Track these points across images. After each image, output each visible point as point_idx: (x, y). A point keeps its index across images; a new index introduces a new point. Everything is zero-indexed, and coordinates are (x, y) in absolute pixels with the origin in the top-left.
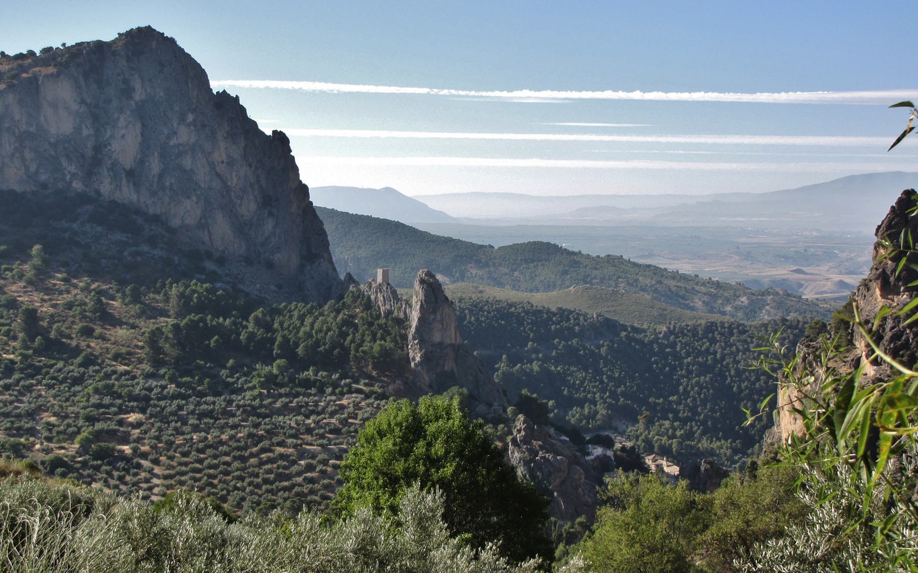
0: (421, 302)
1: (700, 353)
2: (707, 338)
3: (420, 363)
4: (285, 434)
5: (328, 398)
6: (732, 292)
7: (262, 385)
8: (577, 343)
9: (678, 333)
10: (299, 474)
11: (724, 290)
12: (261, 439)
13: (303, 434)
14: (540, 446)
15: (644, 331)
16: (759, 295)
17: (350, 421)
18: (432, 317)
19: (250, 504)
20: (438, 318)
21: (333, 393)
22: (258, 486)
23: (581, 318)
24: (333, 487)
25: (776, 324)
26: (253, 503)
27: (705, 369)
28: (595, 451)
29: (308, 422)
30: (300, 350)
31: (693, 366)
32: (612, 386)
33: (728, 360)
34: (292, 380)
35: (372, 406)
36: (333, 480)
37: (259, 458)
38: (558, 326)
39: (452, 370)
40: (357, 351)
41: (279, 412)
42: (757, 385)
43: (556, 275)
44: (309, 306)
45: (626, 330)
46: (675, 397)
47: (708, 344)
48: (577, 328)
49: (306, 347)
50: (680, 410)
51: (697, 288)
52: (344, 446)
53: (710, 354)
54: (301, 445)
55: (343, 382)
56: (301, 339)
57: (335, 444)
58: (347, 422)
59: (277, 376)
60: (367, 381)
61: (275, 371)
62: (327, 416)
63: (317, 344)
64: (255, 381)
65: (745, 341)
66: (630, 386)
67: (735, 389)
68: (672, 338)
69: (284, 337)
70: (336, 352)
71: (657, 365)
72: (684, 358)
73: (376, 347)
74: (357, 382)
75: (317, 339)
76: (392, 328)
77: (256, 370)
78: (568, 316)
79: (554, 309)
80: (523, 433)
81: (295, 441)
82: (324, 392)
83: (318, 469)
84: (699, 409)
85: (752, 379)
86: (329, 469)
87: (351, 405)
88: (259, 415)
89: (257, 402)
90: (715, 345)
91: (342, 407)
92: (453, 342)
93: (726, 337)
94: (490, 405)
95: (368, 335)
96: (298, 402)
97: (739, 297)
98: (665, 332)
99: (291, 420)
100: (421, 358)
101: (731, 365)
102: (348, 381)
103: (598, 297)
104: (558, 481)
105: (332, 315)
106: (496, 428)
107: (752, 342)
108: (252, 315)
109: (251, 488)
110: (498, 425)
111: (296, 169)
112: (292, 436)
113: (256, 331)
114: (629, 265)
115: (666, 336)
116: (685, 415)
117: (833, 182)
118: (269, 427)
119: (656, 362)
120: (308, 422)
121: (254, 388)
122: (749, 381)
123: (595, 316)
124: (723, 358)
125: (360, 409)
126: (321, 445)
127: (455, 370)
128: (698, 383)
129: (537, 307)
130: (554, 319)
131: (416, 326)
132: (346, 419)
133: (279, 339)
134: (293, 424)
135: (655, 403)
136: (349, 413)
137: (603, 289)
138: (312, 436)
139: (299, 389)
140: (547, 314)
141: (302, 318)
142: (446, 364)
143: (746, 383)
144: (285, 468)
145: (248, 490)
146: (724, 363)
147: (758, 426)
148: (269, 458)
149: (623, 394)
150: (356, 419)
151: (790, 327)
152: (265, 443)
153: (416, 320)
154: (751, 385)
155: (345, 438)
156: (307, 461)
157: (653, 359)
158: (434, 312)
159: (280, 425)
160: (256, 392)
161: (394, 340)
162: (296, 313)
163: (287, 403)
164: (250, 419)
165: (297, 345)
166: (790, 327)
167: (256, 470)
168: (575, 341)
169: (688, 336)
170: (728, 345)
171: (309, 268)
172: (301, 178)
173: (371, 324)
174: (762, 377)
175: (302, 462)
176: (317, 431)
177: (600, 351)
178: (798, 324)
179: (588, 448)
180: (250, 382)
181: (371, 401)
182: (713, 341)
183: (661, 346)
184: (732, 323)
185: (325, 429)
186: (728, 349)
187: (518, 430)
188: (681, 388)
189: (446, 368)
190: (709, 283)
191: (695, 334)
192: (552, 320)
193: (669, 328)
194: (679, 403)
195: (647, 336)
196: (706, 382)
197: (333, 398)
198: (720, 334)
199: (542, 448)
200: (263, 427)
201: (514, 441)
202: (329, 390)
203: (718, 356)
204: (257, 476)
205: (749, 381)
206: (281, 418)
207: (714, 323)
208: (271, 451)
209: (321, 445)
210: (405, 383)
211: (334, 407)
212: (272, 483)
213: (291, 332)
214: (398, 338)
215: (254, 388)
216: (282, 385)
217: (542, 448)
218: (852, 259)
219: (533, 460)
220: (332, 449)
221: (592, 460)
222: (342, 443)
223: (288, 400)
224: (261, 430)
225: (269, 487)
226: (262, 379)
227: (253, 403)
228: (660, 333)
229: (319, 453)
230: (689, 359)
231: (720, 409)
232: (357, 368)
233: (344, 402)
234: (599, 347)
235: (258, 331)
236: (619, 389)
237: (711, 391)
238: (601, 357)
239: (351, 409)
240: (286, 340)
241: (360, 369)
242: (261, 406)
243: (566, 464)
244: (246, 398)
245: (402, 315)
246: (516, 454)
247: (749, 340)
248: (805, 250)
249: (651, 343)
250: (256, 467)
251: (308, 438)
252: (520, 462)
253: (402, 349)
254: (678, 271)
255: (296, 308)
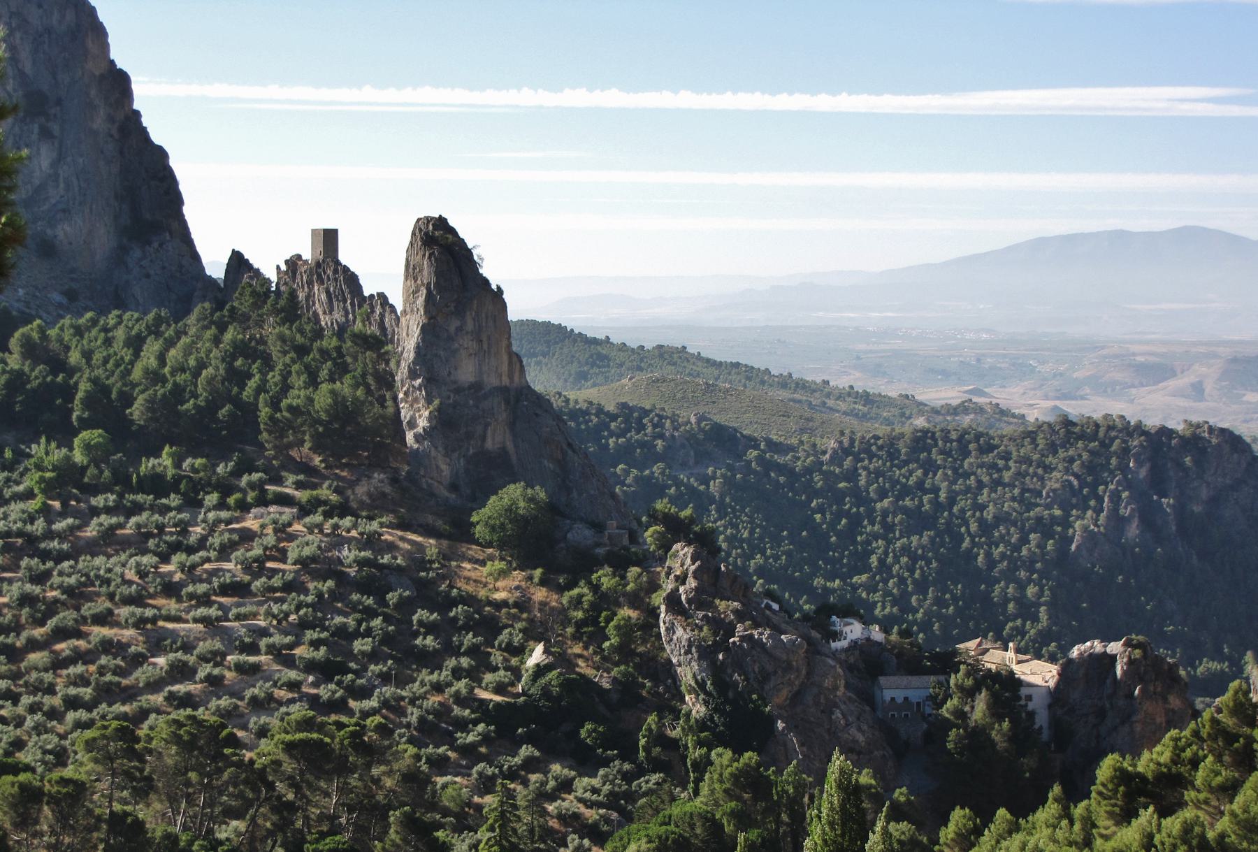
0: (428, 289)
1: (905, 491)
2: (917, 461)
3: (428, 434)
4: (111, 596)
5: (211, 515)
6: (896, 411)
7: (50, 488)
8: (663, 473)
9: (859, 453)
10: (154, 686)
11: (878, 407)
12: (52, 608)
13: (152, 596)
14: (735, 612)
15: (791, 449)
16: (948, 413)
17: (269, 565)
18: (454, 324)
19: (39, 756)
20: (470, 325)
21: (221, 505)
22: (53, 714)
23: (668, 424)
24: (242, 715)
25: (1054, 432)
26: (45, 752)
27: (919, 522)
28: (847, 629)
29: (164, 568)
30: (137, 411)
31: (895, 515)
32: (738, 556)
33: (962, 503)
34: (122, 481)
35: (321, 531)
36: (242, 699)
37: (52, 652)
38: (621, 440)
39: (504, 449)
40: (275, 404)
41: (93, 548)
42: (1024, 552)
43: (566, 381)
44: (151, 316)
45: (756, 447)
46: (864, 577)
47: (919, 472)
48: (659, 443)
49: (151, 404)
50: (875, 603)
51: (830, 403)
52: (262, 623)
53: (925, 492)
54: (154, 620)
55: (245, 479)
56: (137, 385)
57: (238, 617)
58: (262, 568)
59: (84, 469)
60: (301, 477)
61: (79, 457)
62: (213, 554)
63: (178, 394)
64: (28, 482)
65: (994, 466)
66: (772, 556)
67: (980, 559)
68: (848, 462)
69: (95, 381)
70: (223, 412)
71: (824, 515)
72: (876, 502)
73: (322, 398)
74: (279, 481)
75: (175, 384)
76: (355, 359)
77: (29, 456)
78: (640, 419)
79: (611, 407)
80: (692, 583)
81: (138, 611)
82: (200, 504)
83: (201, 674)
84: (914, 599)
85: (1013, 540)
86: (230, 675)
87: (269, 530)
88: (45, 555)
89: (39, 526)
90: (935, 475)
91: (247, 537)
92: (505, 381)
93: (955, 460)
94: (598, 527)
95: (299, 373)
96: (139, 526)
97: (910, 418)
98: (835, 451)
99: (124, 565)
100: (430, 419)
101: (969, 513)
102: (256, 476)
103: (679, 396)
104: (785, 692)
105: (209, 334)
106: (623, 577)
107: (1008, 468)
108: (17, 335)
109: (39, 717)
110: (626, 569)
111: (100, 32)
112: (128, 601)
113: (26, 369)
114: (700, 364)
115: (837, 458)
116: (887, 610)
117: (1009, 249)
118: (72, 580)
119: (821, 510)
120: (164, 568)
121: (29, 495)
122: (1008, 543)
123: (693, 420)
124: (952, 501)
125: (292, 538)
126: (204, 620)
127: (510, 446)
128: (906, 550)
129: (576, 402)
130: (613, 425)
131: (418, 348)
132: (260, 561)
133: (84, 387)
134: (131, 575)
135: (825, 588)
136: (266, 549)
137: (686, 382)
138: (179, 600)
139: (140, 498)
140: (597, 415)
141: (136, 344)
142: (489, 433)
143: (1001, 548)
144: (118, 671)
145: (29, 722)
146: (955, 509)
147: (1033, 632)
148: (75, 650)
149: (761, 571)
150: (284, 561)
151: (1082, 436)
152: (66, 617)
153: (416, 332)
154: (1012, 552)
155: (260, 604)
156: (172, 656)
157: (814, 504)
158: (460, 312)
159: (97, 576)
160: (33, 505)
161: (361, 382)
162: (120, 334)
163: (113, 528)
164: (25, 562)
165: (128, 400)
166: (1082, 436)
167: (48, 677)
168: (657, 469)
169: (879, 458)
170: (959, 474)
171: (137, 253)
172: (114, 55)
173: (302, 351)
174: (1032, 536)
175: (161, 661)
176: (190, 589)
177: (708, 487)
178: (1097, 431)
179: (834, 624)
180: (18, 483)
181: (317, 518)
182: (930, 467)
183: (827, 475)
184: (966, 432)
185: (210, 583)
186: (961, 481)
187: (677, 578)
188: (874, 560)
189: (489, 444)
190: (849, 394)
191: (893, 454)
192: (607, 427)
193: (841, 443)
194: (872, 589)
195: (798, 458)
196: (923, 548)
197: (224, 514)
198: (941, 452)
199: (740, 616)
200: (56, 579)
201: (673, 601)
202: (212, 499)
203: (943, 495)
204: (51, 690)
205: (1008, 543)
206: (99, 561)
207: (928, 431)
208: (79, 635)
209: (204, 620)
210: (394, 481)
211: (226, 536)
212: (90, 707)
213: (113, 373)
214: (370, 380)
215: (29, 495)
216: (95, 490)
217: (740, 616)
218: (1061, 375)
219: (721, 645)
220: (232, 628)
221: (846, 650)
222: (254, 615)
223: (114, 520)
224: (52, 588)
225: (82, 715)
226: (48, 475)
227: (29, 527)
228: (824, 453)
229: (199, 639)
230: (886, 503)
231: (955, 599)
232: (275, 447)
233: (251, 523)
234: (706, 480)
235: (32, 370)
236: (753, 562)
237: (934, 565)
238: (712, 500)
239: (270, 540)
240: (100, 389)
241: (282, 449)
242: (49, 535)
243: (801, 652)
244: (11, 518)
245: (374, 329)
246: (680, 632)
247: (1001, 463)
248: (978, 360)
249: (808, 471)
250: (46, 670)
251: (171, 605)
252: (688, 652)
253: (382, 401)
254: (790, 375)
255: (120, 323)
